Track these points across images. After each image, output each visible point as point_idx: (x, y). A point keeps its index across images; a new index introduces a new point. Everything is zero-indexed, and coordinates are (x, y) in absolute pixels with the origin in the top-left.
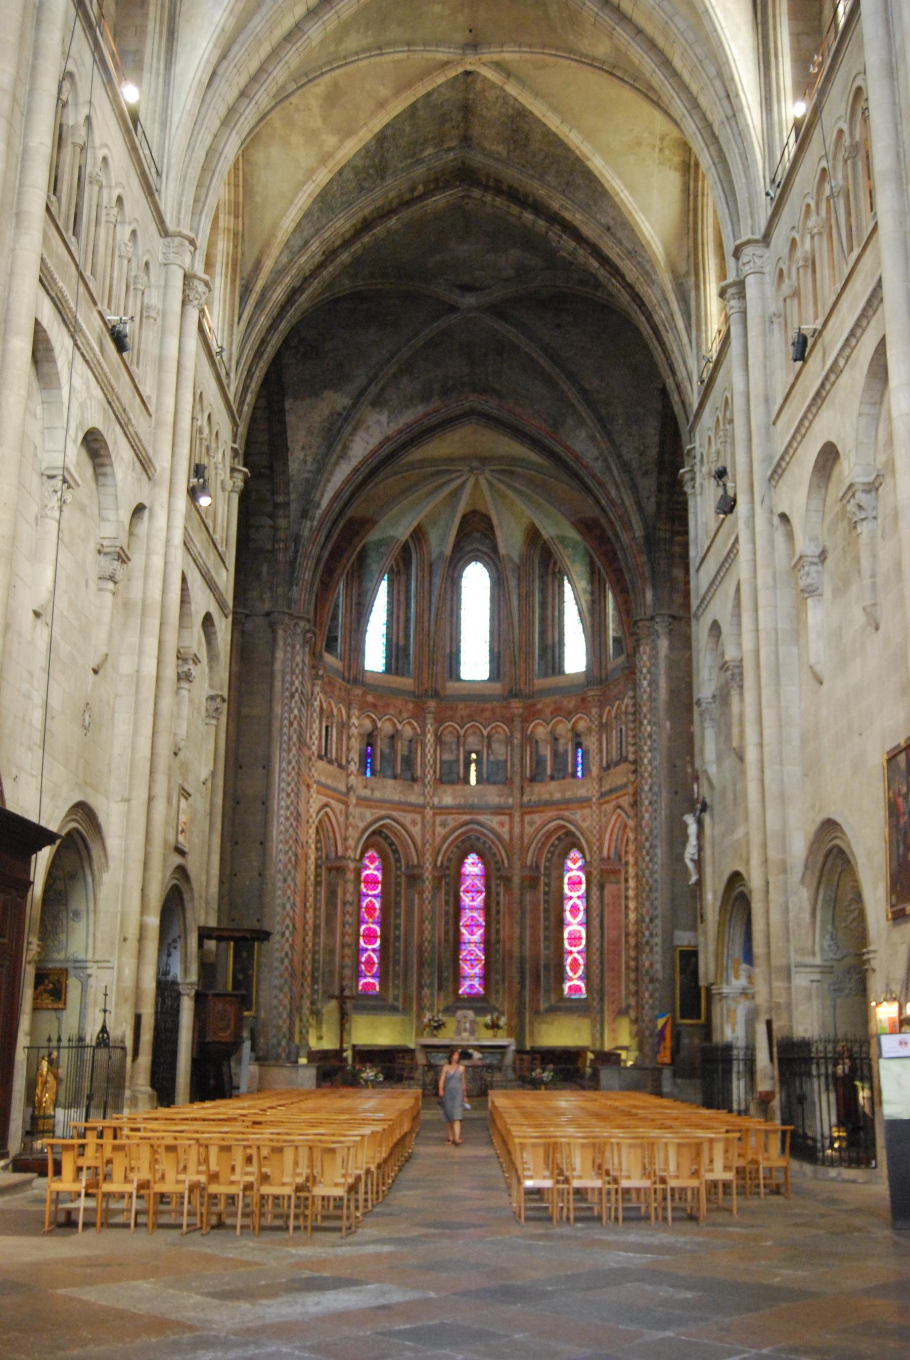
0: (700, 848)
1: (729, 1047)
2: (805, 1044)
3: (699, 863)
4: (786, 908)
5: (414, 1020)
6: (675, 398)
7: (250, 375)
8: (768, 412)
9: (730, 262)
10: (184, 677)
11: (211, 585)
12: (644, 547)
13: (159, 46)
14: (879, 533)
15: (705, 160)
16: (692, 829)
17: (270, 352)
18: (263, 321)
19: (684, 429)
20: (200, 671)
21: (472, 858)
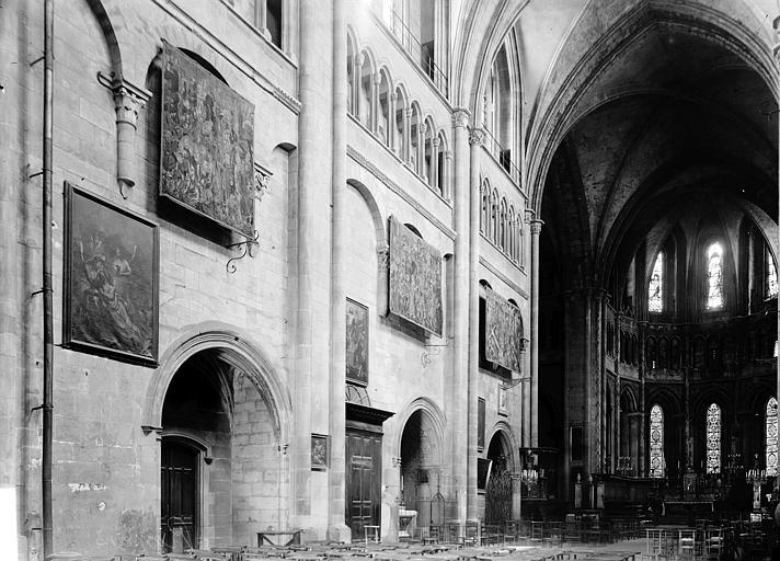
21: (714, 406)
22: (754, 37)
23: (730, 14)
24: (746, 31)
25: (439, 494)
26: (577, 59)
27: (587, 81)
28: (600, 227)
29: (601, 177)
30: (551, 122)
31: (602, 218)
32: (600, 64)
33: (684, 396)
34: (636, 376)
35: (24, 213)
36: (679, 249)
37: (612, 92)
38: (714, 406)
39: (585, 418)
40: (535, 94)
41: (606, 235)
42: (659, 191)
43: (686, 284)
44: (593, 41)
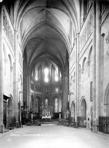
0: (70, 99)
1: (72, 117)
2: (80, 117)
3: (69, 100)
4: (79, 104)
5: (30, 23)
6: (68, 51)
7: (23, 47)
8: (82, 48)
9: (75, 36)
10: (19, 81)
11: (21, 72)
12: (64, 67)
13: (18, 26)
14: (73, 77)
15: (73, 23)
16: (69, 97)
17: (25, 45)
18: (25, 41)
19: (69, 55)
20: (20, 80)
21: (46, 99)
22: (64, 34)
23: (60, 28)
24: (63, 33)
25: (91, 128)
26: (32, 27)
27: (33, 32)
28: (29, 61)
29: (30, 52)
30: (26, 38)
31: (30, 60)
32: (36, 29)
33: (42, 97)
34: (33, 92)
35: (95, 27)
36: (41, 69)
37: (36, 36)
38: (46, 99)
39: (26, 100)
40: (24, 31)
41: (30, 63)
42: (40, 57)
43: (41, 76)
44: (35, 24)
